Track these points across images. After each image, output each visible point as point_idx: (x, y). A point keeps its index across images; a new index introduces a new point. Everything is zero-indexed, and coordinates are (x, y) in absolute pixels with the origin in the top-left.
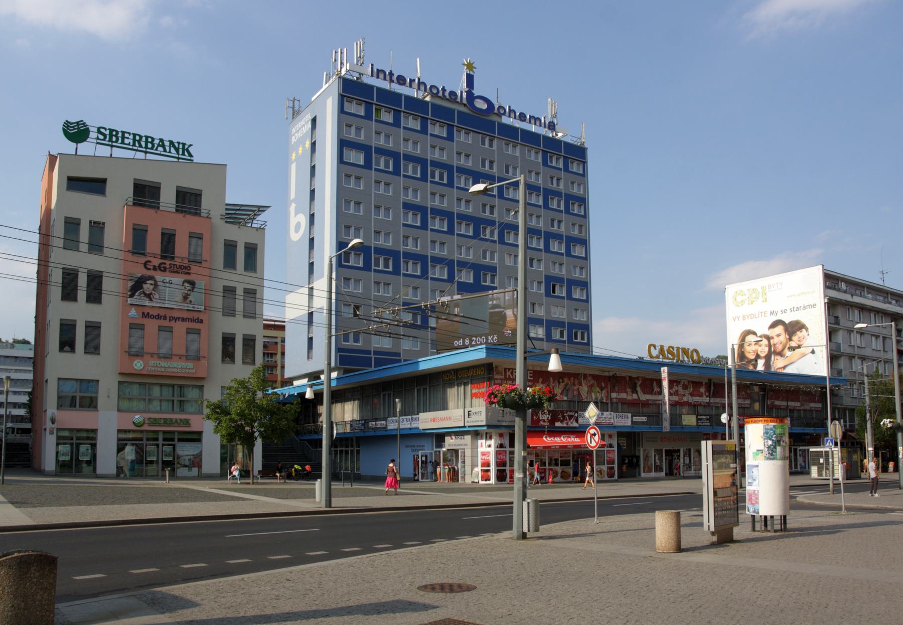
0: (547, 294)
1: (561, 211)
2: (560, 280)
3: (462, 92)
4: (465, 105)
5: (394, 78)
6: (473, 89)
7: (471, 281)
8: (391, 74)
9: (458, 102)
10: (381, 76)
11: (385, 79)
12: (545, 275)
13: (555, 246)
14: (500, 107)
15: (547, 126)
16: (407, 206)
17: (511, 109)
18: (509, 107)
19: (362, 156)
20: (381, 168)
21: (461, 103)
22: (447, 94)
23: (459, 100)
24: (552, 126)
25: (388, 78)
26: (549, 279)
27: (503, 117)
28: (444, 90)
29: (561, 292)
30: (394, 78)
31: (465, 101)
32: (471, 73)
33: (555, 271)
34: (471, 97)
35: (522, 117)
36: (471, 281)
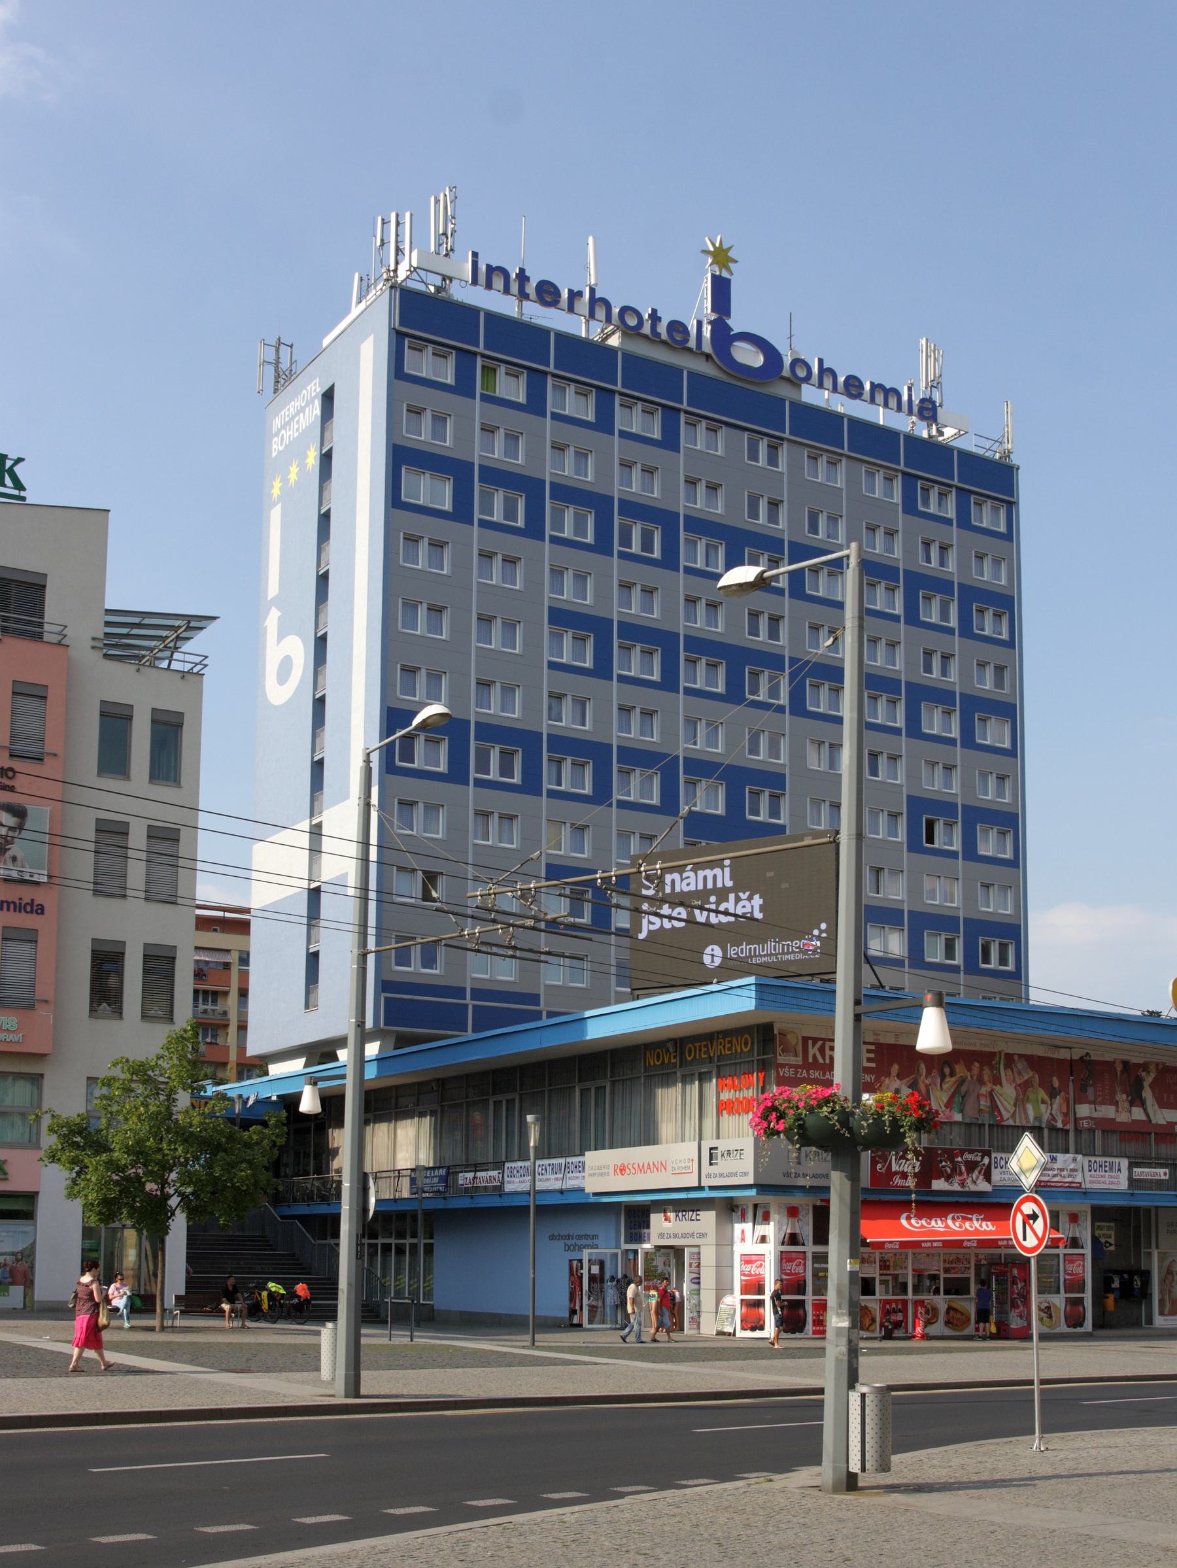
0: (914, 846)
1: (950, 631)
2: (947, 808)
3: (700, 324)
4: (708, 357)
5: (531, 289)
6: (729, 315)
7: (720, 811)
8: (522, 277)
9: (690, 350)
10: (498, 282)
11: (507, 290)
12: (908, 796)
13: (934, 722)
14: (796, 362)
15: (915, 409)
16: (561, 618)
17: (597, 296)
18: (821, 361)
19: (448, 489)
20: (565, 535)
21: (698, 353)
22: (662, 329)
23: (692, 344)
24: (928, 411)
25: (514, 287)
26: (917, 805)
27: (804, 386)
28: (655, 317)
29: (949, 838)
30: (531, 289)
31: (707, 347)
32: (725, 274)
33: (934, 785)
34: (723, 335)
35: (853, 387)
36: (720, 811)
